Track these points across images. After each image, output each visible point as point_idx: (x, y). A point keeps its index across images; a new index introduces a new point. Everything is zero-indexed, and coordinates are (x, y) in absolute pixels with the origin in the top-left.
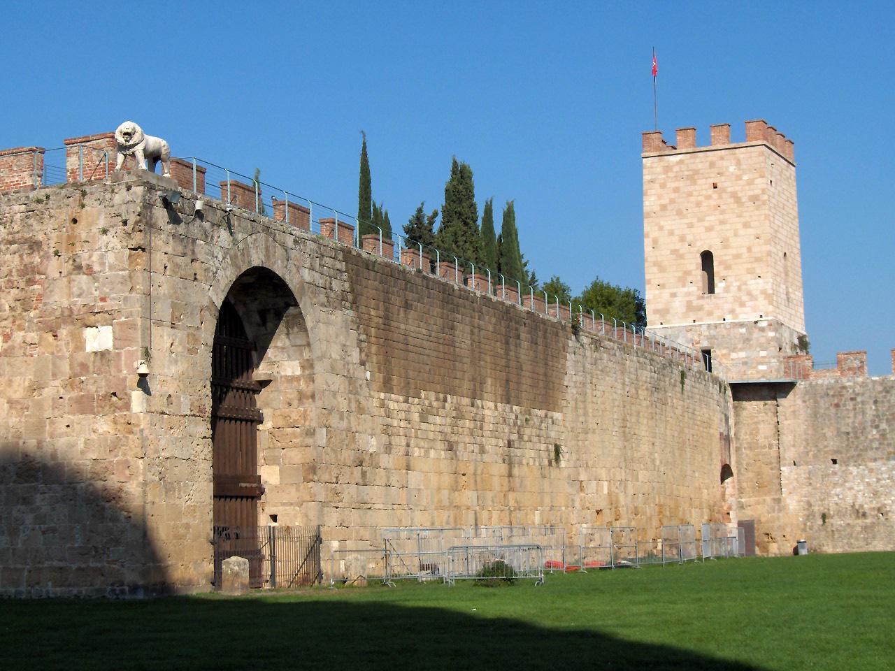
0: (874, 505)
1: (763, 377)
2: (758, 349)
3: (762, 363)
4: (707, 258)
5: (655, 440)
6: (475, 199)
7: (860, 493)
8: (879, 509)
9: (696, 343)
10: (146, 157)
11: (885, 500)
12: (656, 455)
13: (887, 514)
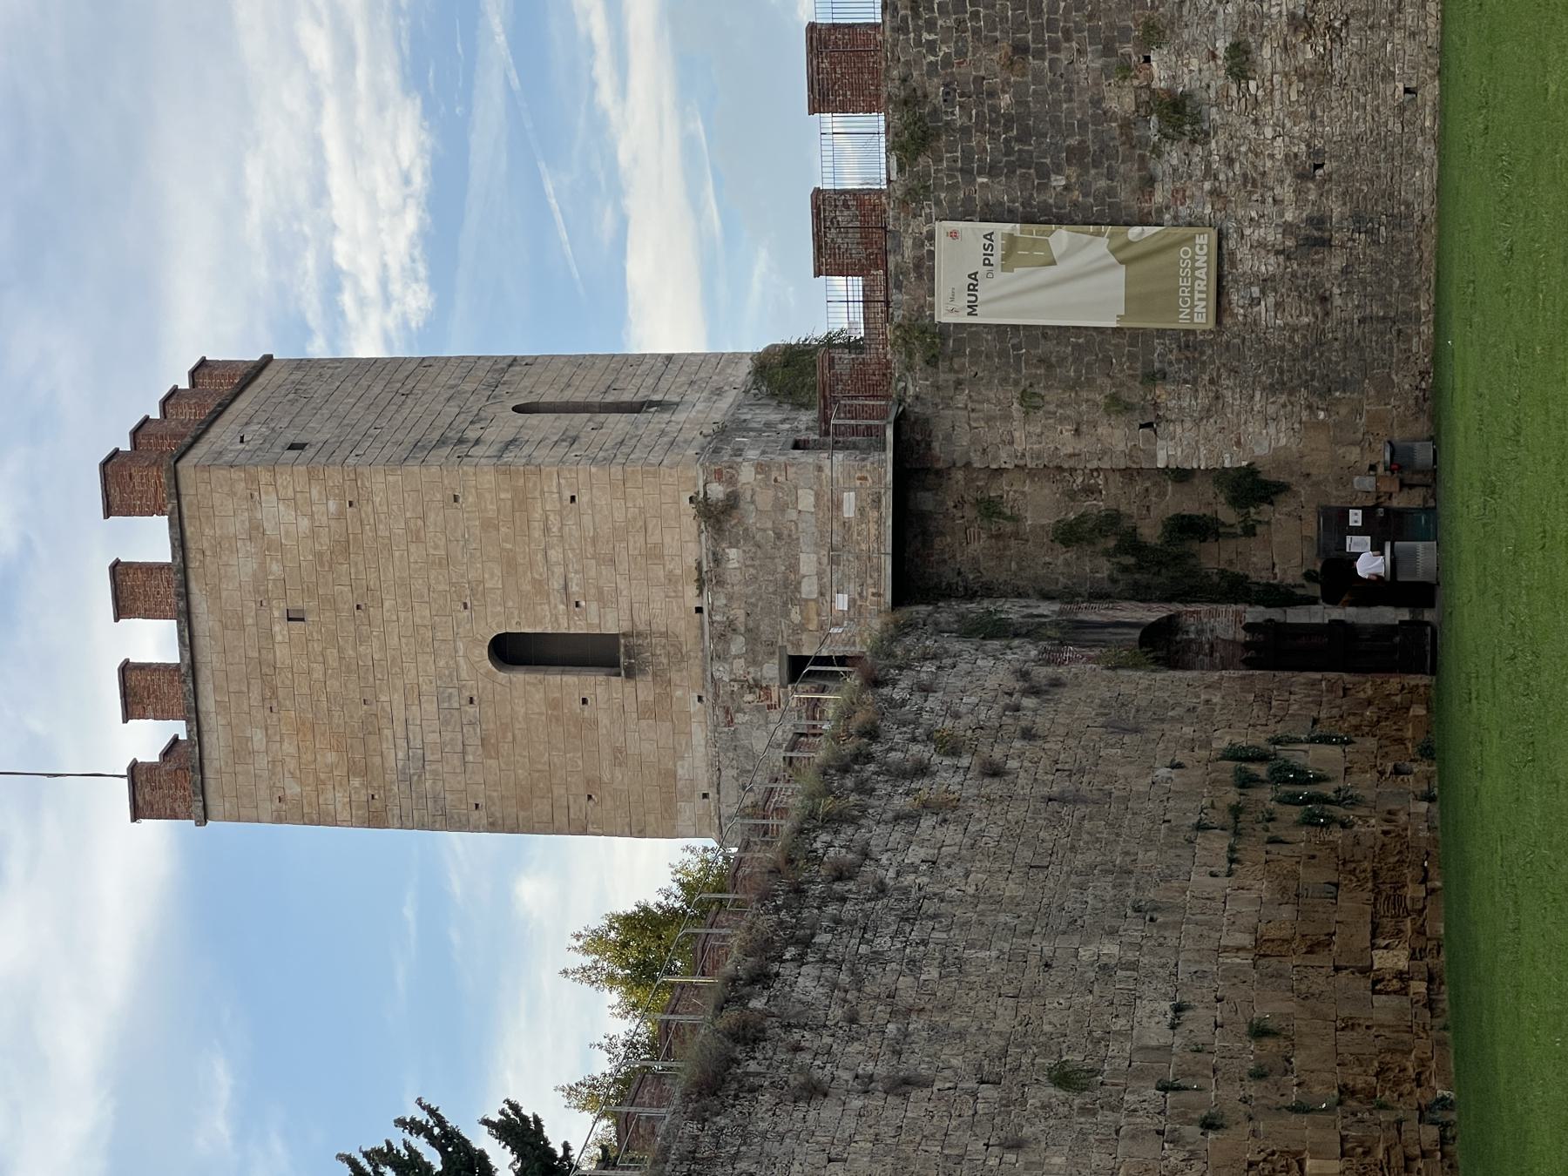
0: (1286, 192)
1: (877, 502)
2: (793, 515)
3: (837, 505)
4: (510, 651)
5: (1033, 960)
6: (653, 899)
7: (1247, 232)
8: (1303, 176)
9: (769, 697)
10: (1170, 618)
11: (1272, 156)
12: (1085, 954)
13: (1318, 153)
